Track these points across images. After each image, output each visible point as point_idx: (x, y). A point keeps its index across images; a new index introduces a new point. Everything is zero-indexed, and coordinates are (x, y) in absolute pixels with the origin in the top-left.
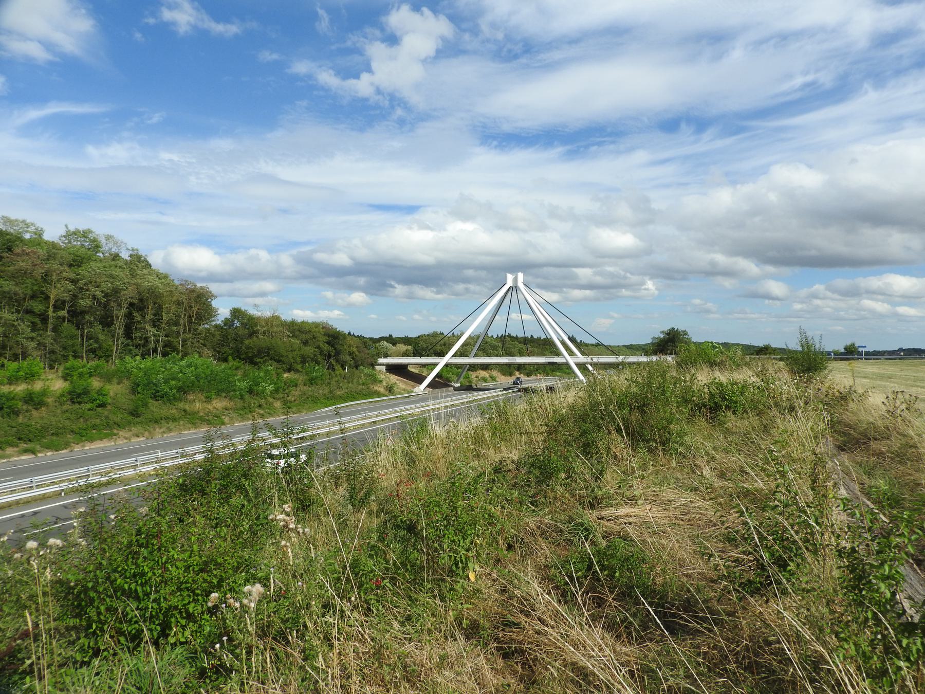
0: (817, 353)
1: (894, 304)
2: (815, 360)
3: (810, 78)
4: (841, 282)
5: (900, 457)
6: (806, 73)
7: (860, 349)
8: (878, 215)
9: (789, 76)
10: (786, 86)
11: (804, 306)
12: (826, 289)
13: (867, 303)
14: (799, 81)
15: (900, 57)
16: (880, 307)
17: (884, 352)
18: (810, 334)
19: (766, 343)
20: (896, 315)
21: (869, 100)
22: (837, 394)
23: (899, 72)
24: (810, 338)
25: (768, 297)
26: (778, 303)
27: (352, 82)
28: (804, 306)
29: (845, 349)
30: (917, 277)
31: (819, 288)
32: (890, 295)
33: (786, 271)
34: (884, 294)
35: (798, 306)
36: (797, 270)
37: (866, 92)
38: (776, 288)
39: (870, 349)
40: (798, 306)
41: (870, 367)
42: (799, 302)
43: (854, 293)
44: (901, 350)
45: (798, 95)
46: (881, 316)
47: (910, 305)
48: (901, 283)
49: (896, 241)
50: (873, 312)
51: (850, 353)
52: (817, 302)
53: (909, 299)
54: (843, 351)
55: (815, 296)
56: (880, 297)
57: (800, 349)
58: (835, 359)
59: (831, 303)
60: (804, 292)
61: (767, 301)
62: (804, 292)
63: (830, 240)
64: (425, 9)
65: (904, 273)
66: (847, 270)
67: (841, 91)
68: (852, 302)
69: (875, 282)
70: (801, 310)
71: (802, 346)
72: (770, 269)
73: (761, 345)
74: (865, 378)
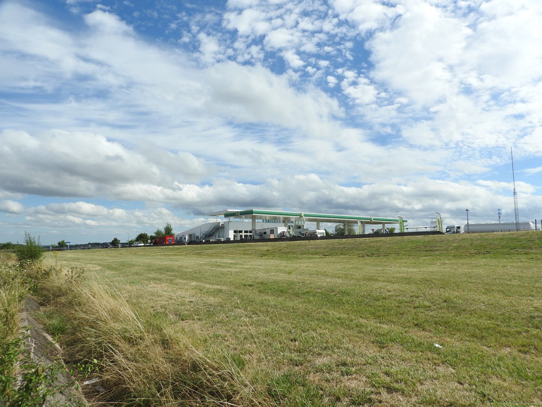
0: (35, 247)
1: (85, 219)
2: (35, 251)
3: (39, 84)
4: (55, 205)
5: (71, 304)
6: (36, 80)
7: (67, 244)
8: (70, 169)
9: (25, 79)
10: (23, 84)
11: (33, 218)
12: (46, 208)
13: (70, 218)
14: (32, 84)
15: (88, 89)
16: (77, 220)
17: (81, 245)
18: (32, 236)
19: (8, 241)
20: (85, 224)
21: (71, 106)
22: (43, 272)
23: (87, 97)
24: (32, 238)
25: (7, 211)
26: (14, 215)
27: (384, 129)
28: (33, 218)
29: (59, 244)
30: (95, 205)
31: (42, 208)
32: (81, 214)
33: (19, 196)
34: (77, 213)
35: (28, 218)
36: (27, 196)
37: (71, 102)
38: (14, 206)
39: (73, 243)
40: (28, 218)
41: (70, 254)
42: (29, 216)
43: (62, 212)
44: (89, 244)
45: (31, 92)
46: (77, 225)
47: (93, 220)
48: (86, 207)
49: (84, 185)
50: (73, 222)
51: (62, 246)
52: (41, 216)
53: (91, 216)
54: (57, 245)
55: (37, 212)
56: (76, 214)
57: (26, 244)
58: (52, 250)
59: (49, 217)
60: (31, 209)
61: (7, 214)
62: (31, 209)
63: (41, 179)
64: (103, 19)
65: (88, 202)
66: (58, 198)
67: (56, 97)
68: (61, 216)
69: (73, 205)
70: (31, 221)
71: (27, 243)
72: (7, 193)
73: (5, 242)
74: (65, 260)
